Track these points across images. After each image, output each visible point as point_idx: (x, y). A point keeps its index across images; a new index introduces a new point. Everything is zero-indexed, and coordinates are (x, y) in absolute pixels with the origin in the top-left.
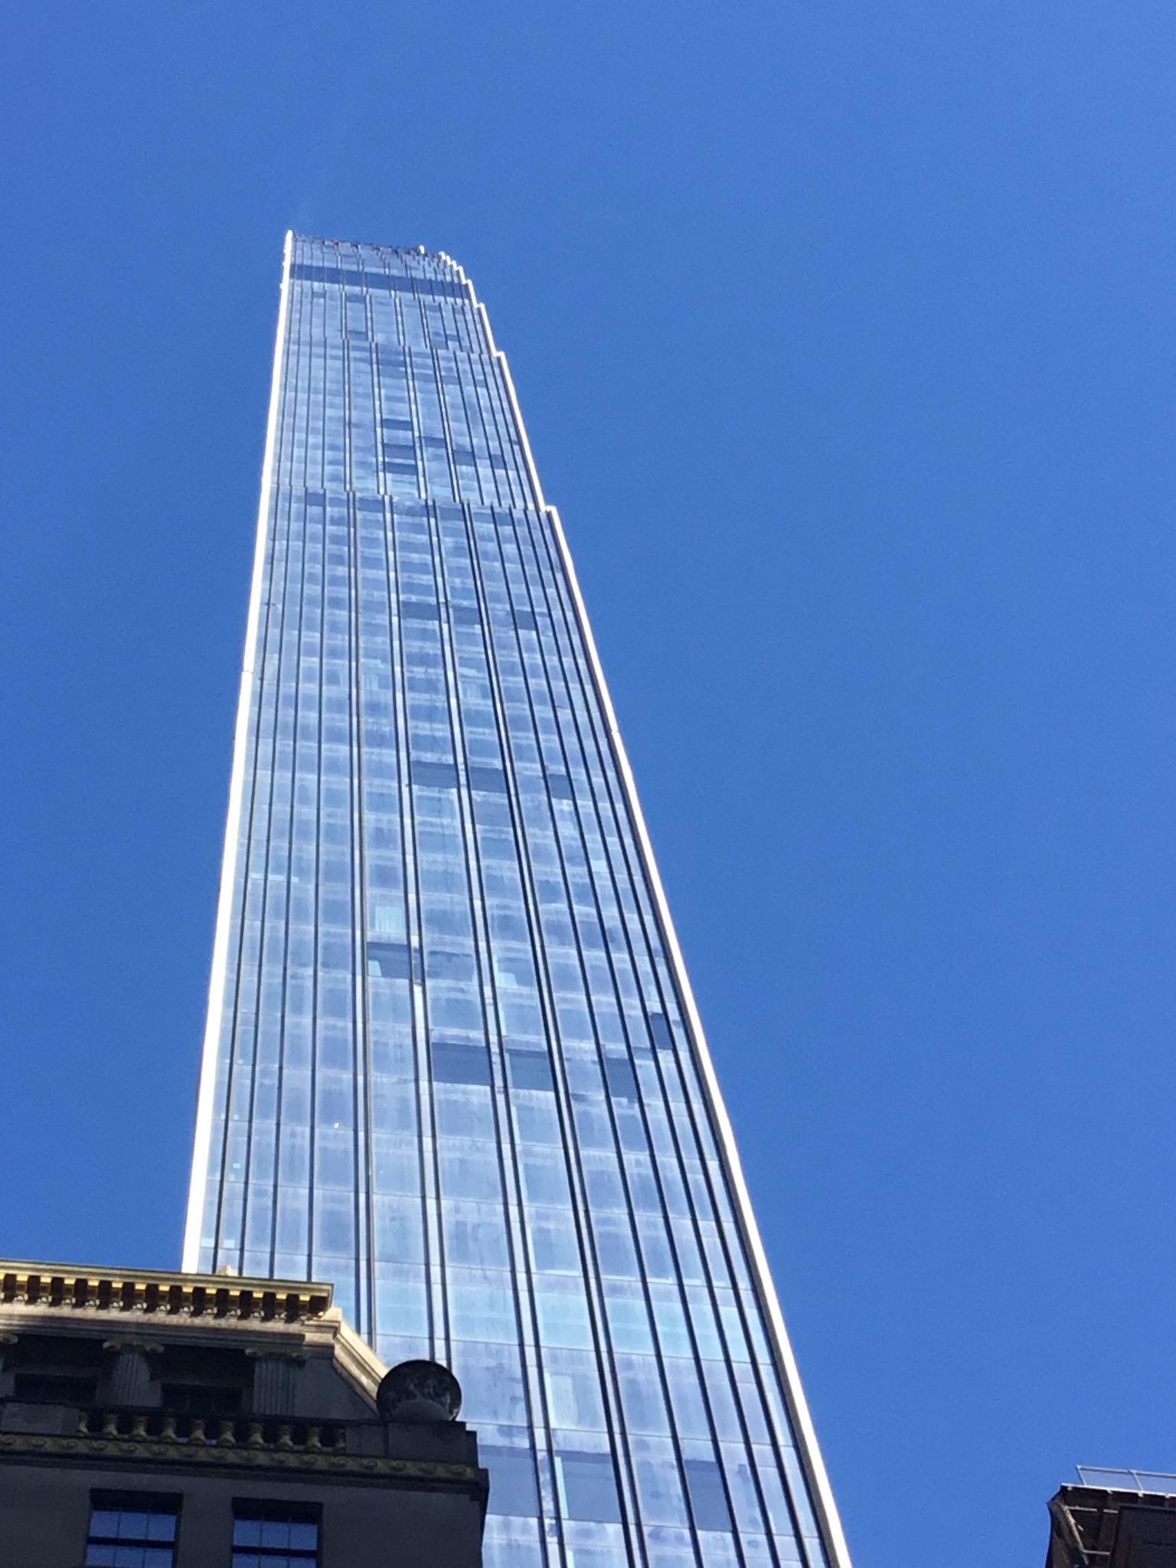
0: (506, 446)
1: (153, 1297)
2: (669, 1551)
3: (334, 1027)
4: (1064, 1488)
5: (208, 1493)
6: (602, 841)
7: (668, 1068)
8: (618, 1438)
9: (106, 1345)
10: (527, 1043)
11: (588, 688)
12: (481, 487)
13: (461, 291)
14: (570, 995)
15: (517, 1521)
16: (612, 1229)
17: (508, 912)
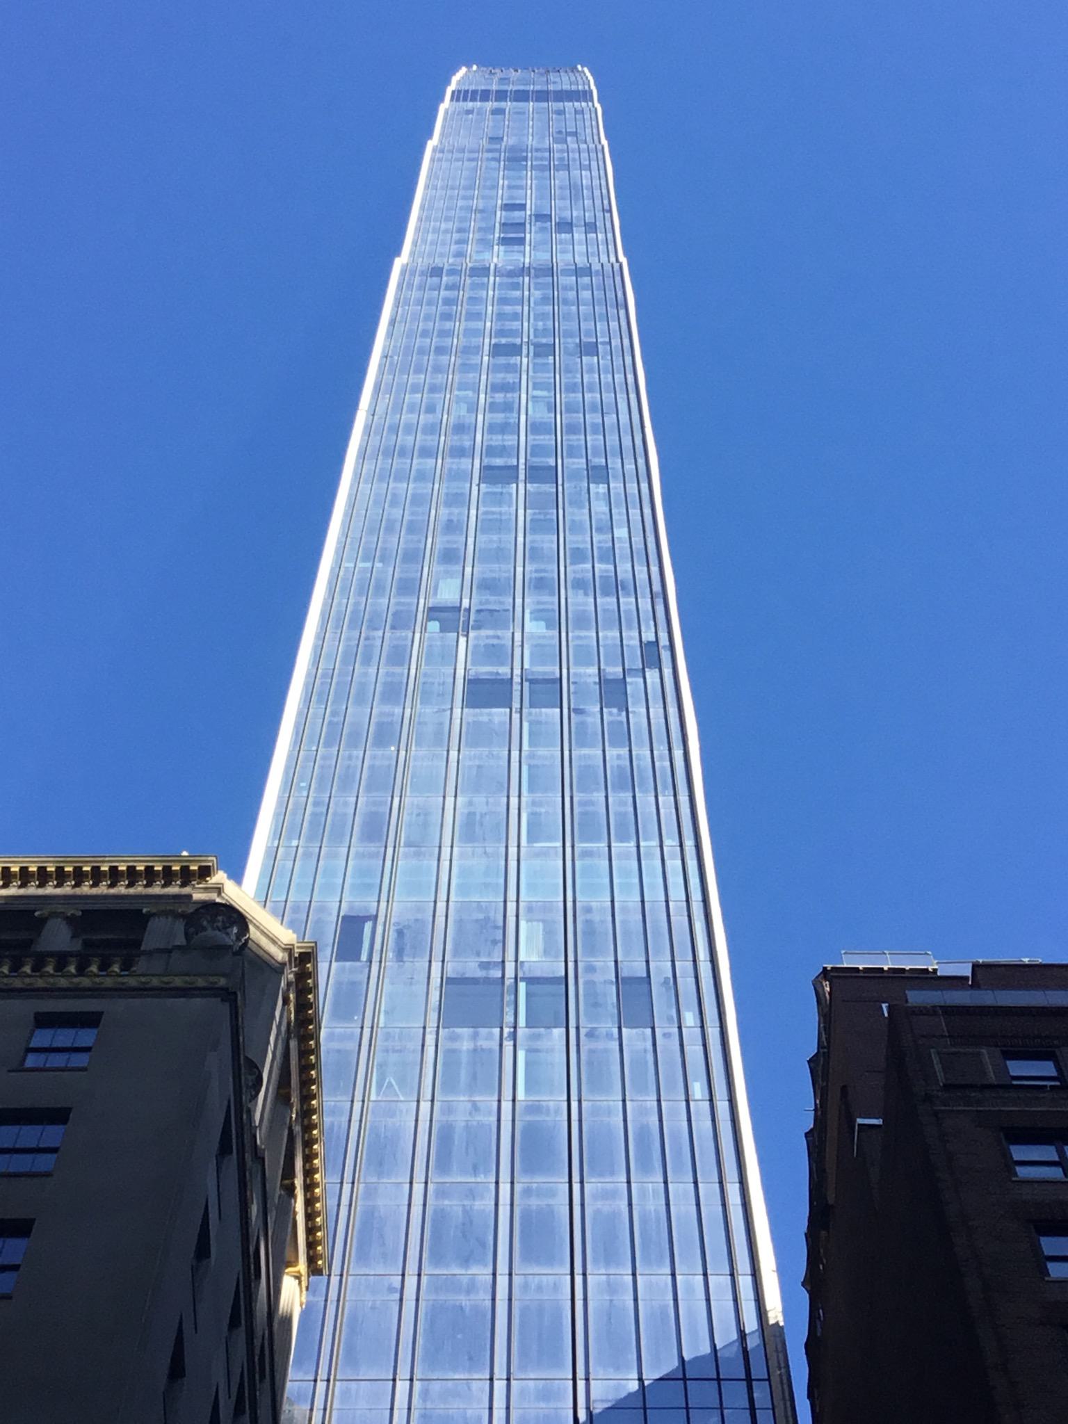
0: (599, 215)
1: (97, 876)
2: (600, 1045)
3: (393, 674)
4: (825, 968)
6: (630, 514)
7: (653, 683)
8: (571, 965)
9: (36, 914)
10: (545, 673)
11: (633, 396)
12: (574, 250)
13: (586, 96)
14: (583, 633)
15: (483, 1031)
16: (590, 809)
17: (542, 575)
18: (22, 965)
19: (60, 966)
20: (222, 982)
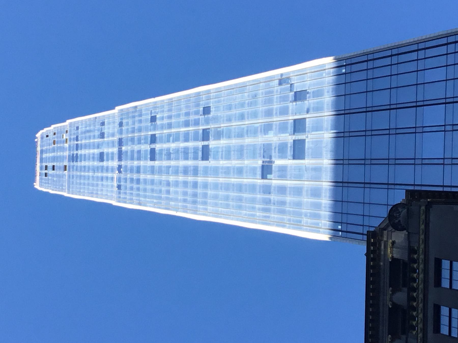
5: (432, 298)
9: (390, 307)
10: (291, 127)
18: (413, 316)
19: (414, 299)
20: (423, 208)
